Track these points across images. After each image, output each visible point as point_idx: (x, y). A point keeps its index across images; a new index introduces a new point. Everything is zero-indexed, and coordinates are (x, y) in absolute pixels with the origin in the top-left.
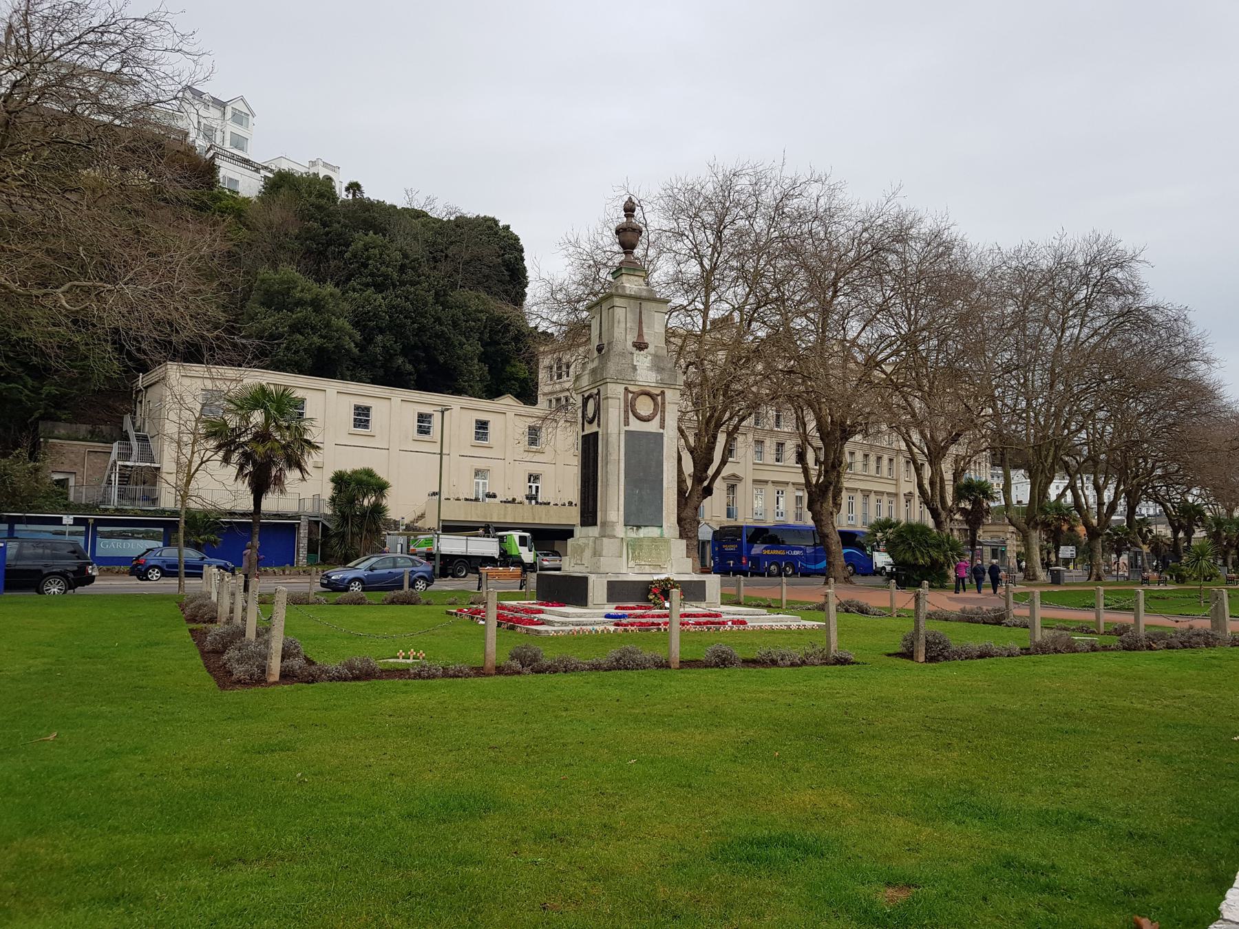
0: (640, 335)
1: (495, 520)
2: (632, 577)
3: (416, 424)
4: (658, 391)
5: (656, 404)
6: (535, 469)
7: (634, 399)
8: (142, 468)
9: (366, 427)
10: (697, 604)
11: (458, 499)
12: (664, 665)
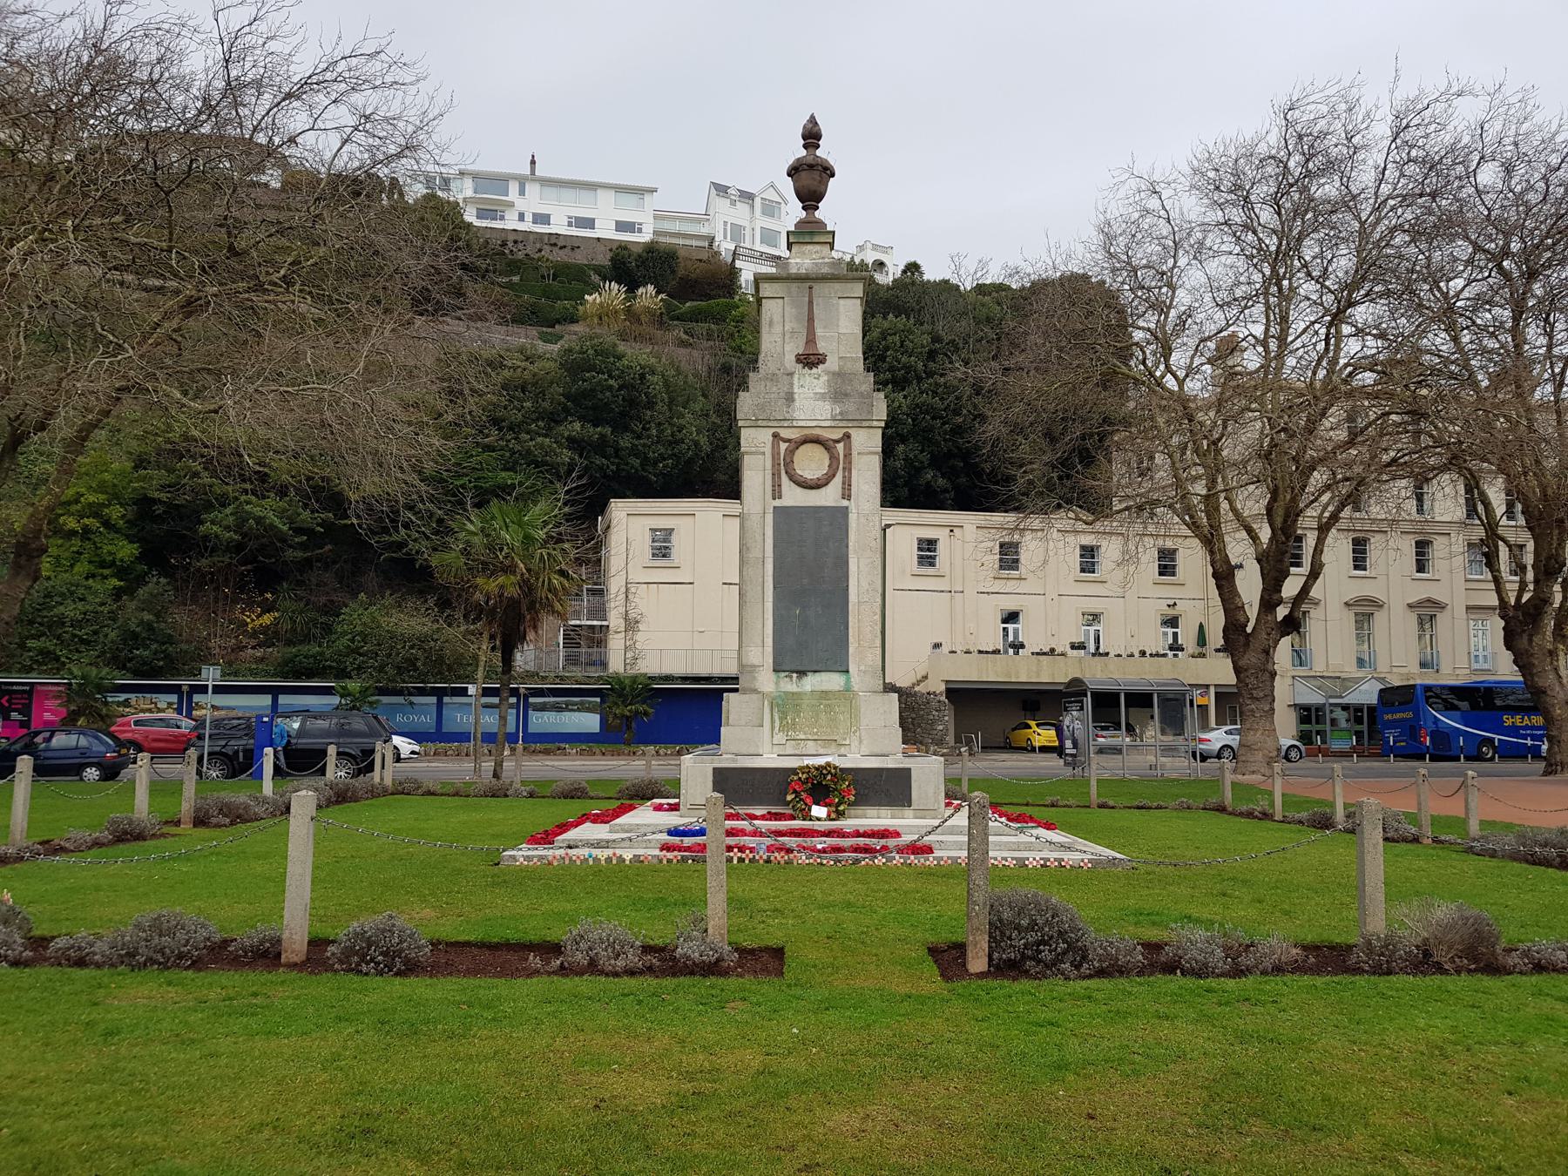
0: (811, 340)
1: (1023, 679)
2: (769, 759)
3: (916, 552)
4: (837, 435)
5: (834, 458)
6: (1094, 605)
7: (791, 453)
8: (592, 627)
9: (932, 565)
10: (897, 811)
11: (968, 652)
12: (267, 955)
